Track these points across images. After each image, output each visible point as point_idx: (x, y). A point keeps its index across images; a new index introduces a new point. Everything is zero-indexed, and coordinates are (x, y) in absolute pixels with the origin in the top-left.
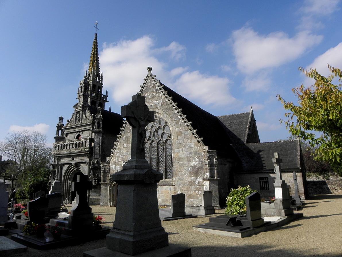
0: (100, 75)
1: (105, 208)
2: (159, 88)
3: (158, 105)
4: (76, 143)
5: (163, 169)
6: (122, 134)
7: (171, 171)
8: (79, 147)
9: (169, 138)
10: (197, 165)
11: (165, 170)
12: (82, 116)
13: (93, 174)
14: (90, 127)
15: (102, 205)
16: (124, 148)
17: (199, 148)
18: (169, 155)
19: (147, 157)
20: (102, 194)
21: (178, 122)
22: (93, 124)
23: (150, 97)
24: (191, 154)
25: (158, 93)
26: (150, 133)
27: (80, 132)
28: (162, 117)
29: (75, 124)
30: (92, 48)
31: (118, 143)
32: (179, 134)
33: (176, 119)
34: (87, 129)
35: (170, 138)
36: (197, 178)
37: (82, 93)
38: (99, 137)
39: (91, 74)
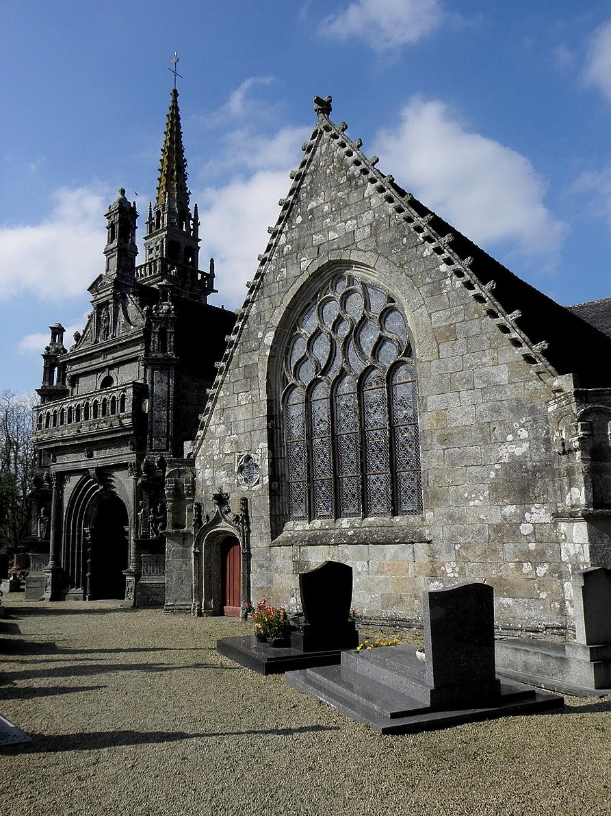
0: (192, 212)
1: (180, 620)
2: (360, 167)
3: (359, 236)
4: (96, 402)
5: (382, 477)
6: (232, 356)
7: (414, 486)
8: (104, 414)
9: (405, 355)
10: (524, 455)
11: (392, 482)
12: (116, 315)
13: (147, 502)
14: (139, 348)
15: (170, 611)
17: (534, 384)
18: (406, 422)
19: (322, 435)
20: (171, 571)
21: (437, 288)
22: (146, 338)
23: (326, 208)
24: (497, 411)
25: (357, 187)
26: (332, 346)
27: (111, 367)
28: (372, 278)
29: (96, 342)
30: (166, 133)
31: (218, 393)
32: (448, 334)
33: (428, 280)
34: (130, 357)
35: (406, 359)
36: (529, 511)
37: (115, 243)
38: (166, 381)
39: (163, 210)
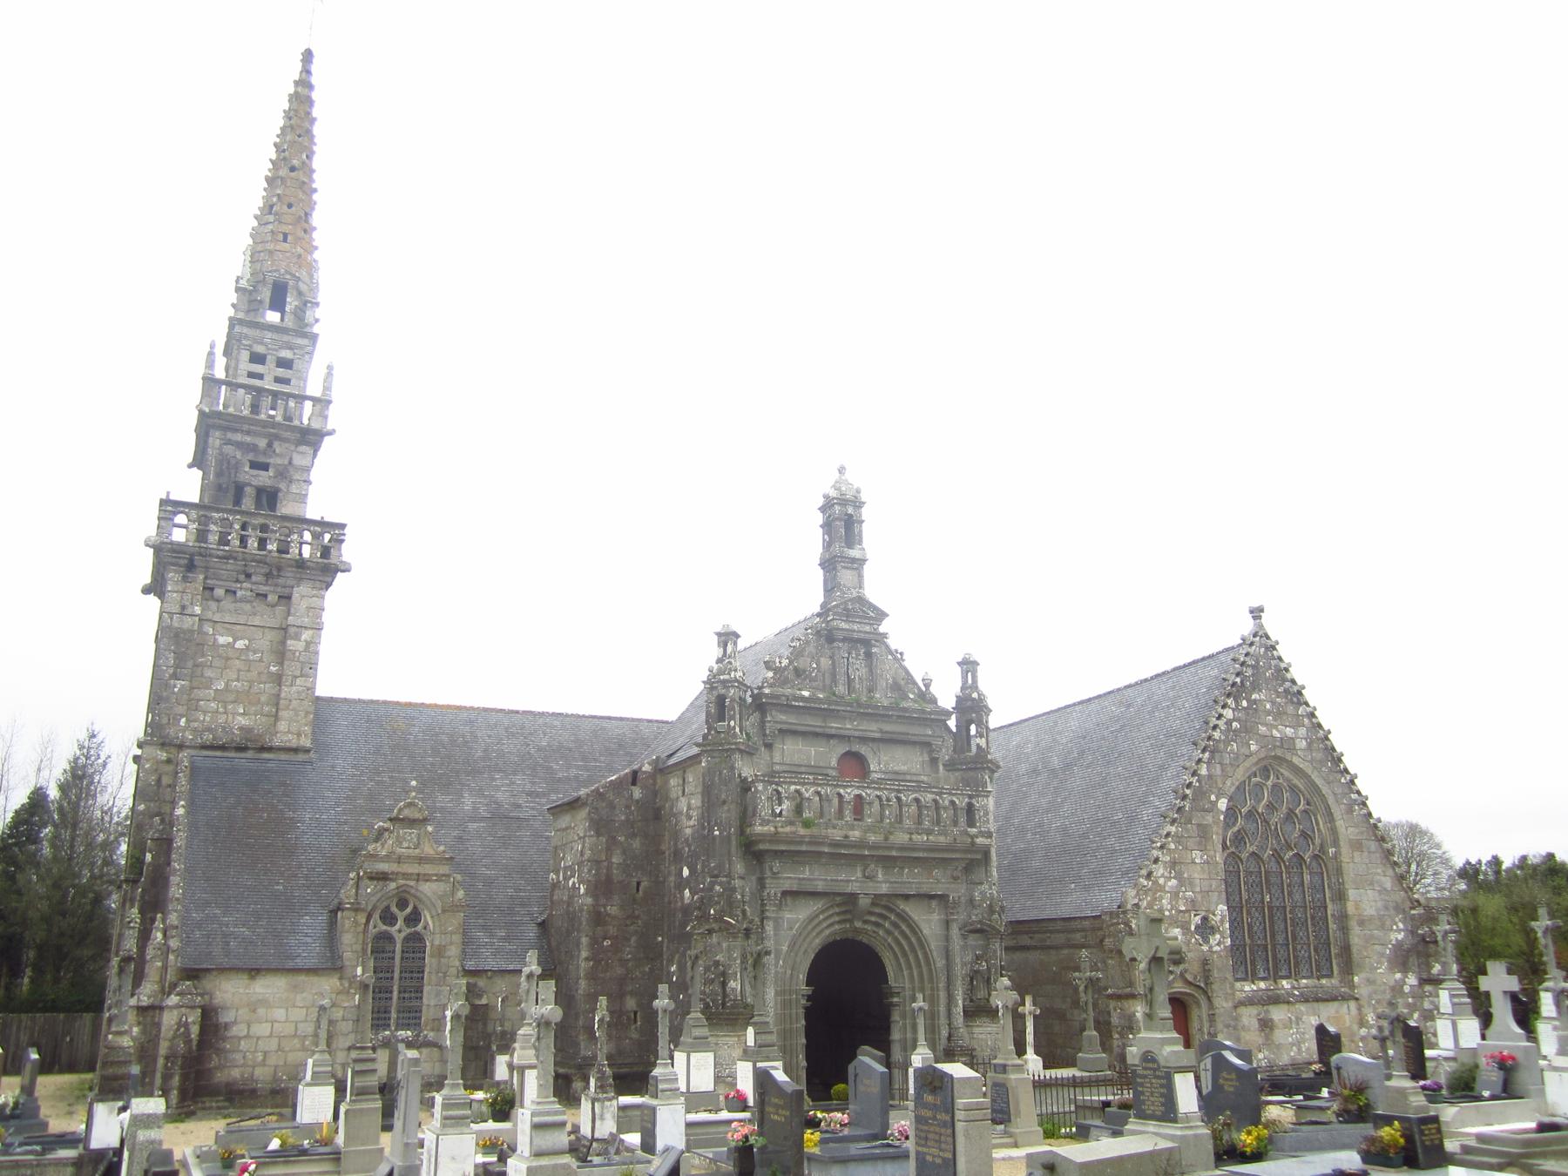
16: (1193, 862)
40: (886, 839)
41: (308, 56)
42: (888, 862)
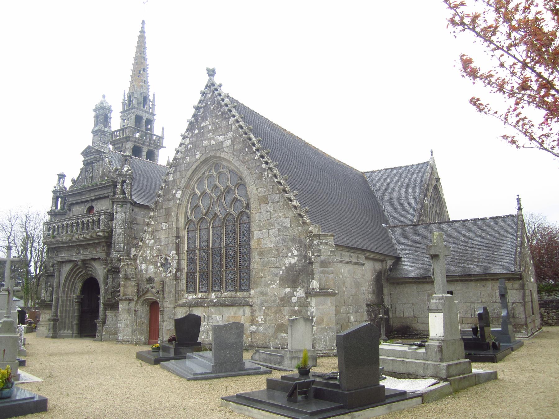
16: (162, 230)
40: (72, 239)
41: (143, 22)
42: (83, 247)
